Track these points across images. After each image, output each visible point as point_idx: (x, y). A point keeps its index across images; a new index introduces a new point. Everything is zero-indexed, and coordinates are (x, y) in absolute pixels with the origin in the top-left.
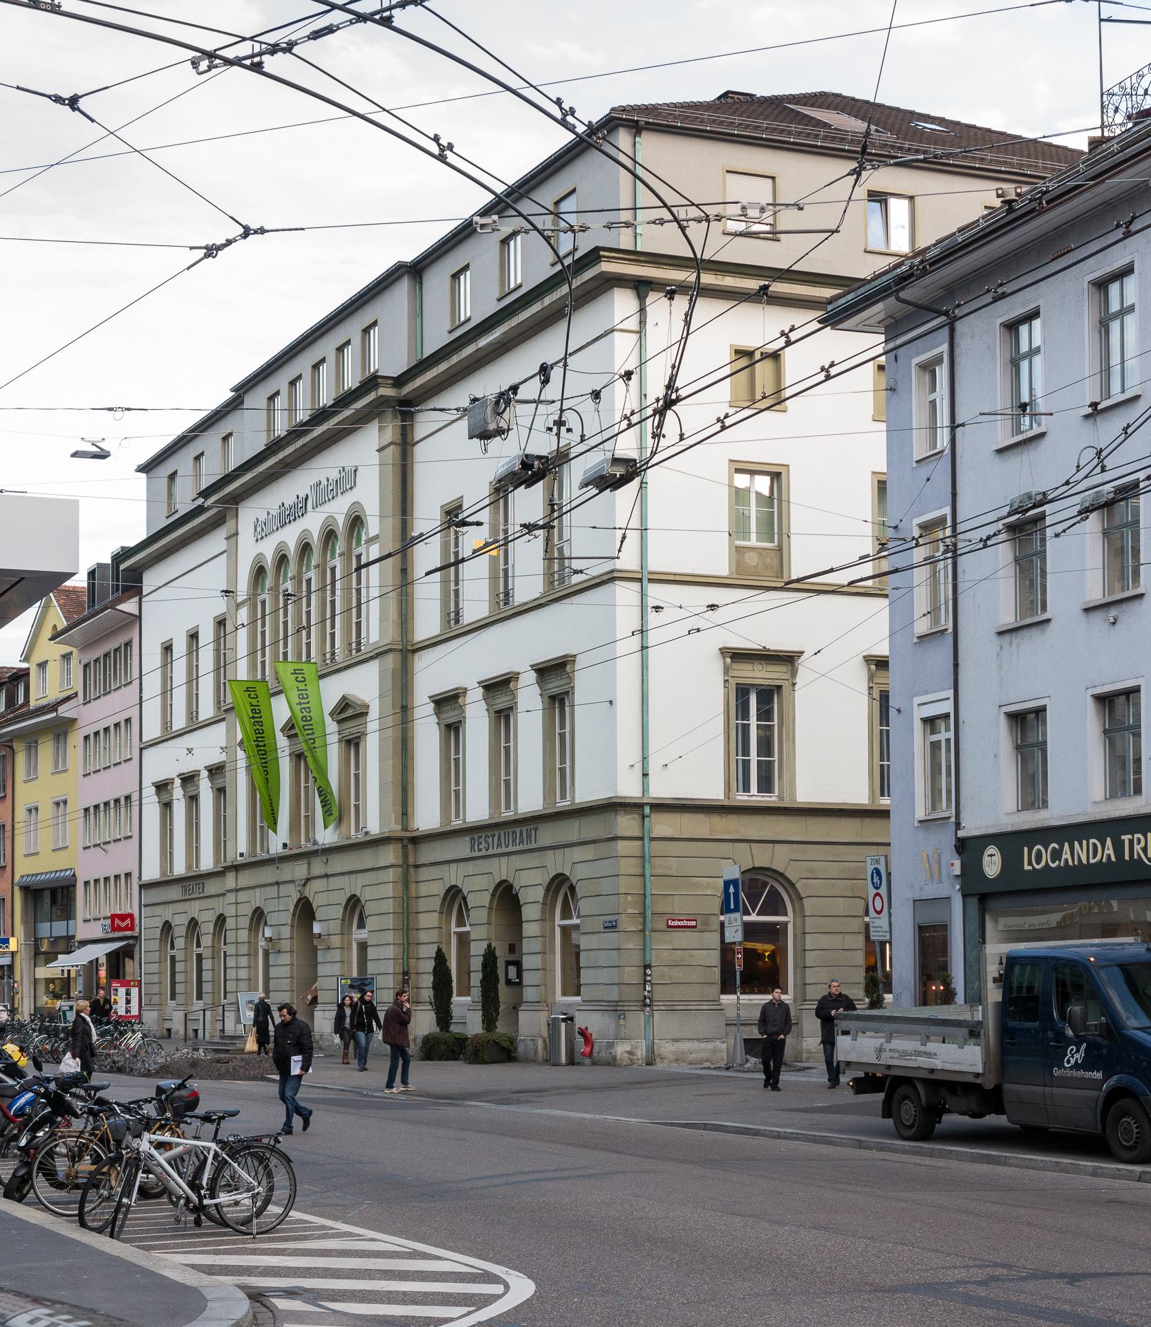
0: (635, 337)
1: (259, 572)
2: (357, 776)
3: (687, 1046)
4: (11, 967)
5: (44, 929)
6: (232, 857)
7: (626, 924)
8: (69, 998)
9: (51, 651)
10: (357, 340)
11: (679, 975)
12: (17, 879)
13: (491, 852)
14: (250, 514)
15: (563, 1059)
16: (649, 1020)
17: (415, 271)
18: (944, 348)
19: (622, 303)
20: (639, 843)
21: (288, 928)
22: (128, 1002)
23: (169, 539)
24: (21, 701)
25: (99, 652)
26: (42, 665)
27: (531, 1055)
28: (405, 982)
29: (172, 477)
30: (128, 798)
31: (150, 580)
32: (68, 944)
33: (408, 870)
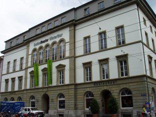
1: (35, 50)
33: (76, 89)
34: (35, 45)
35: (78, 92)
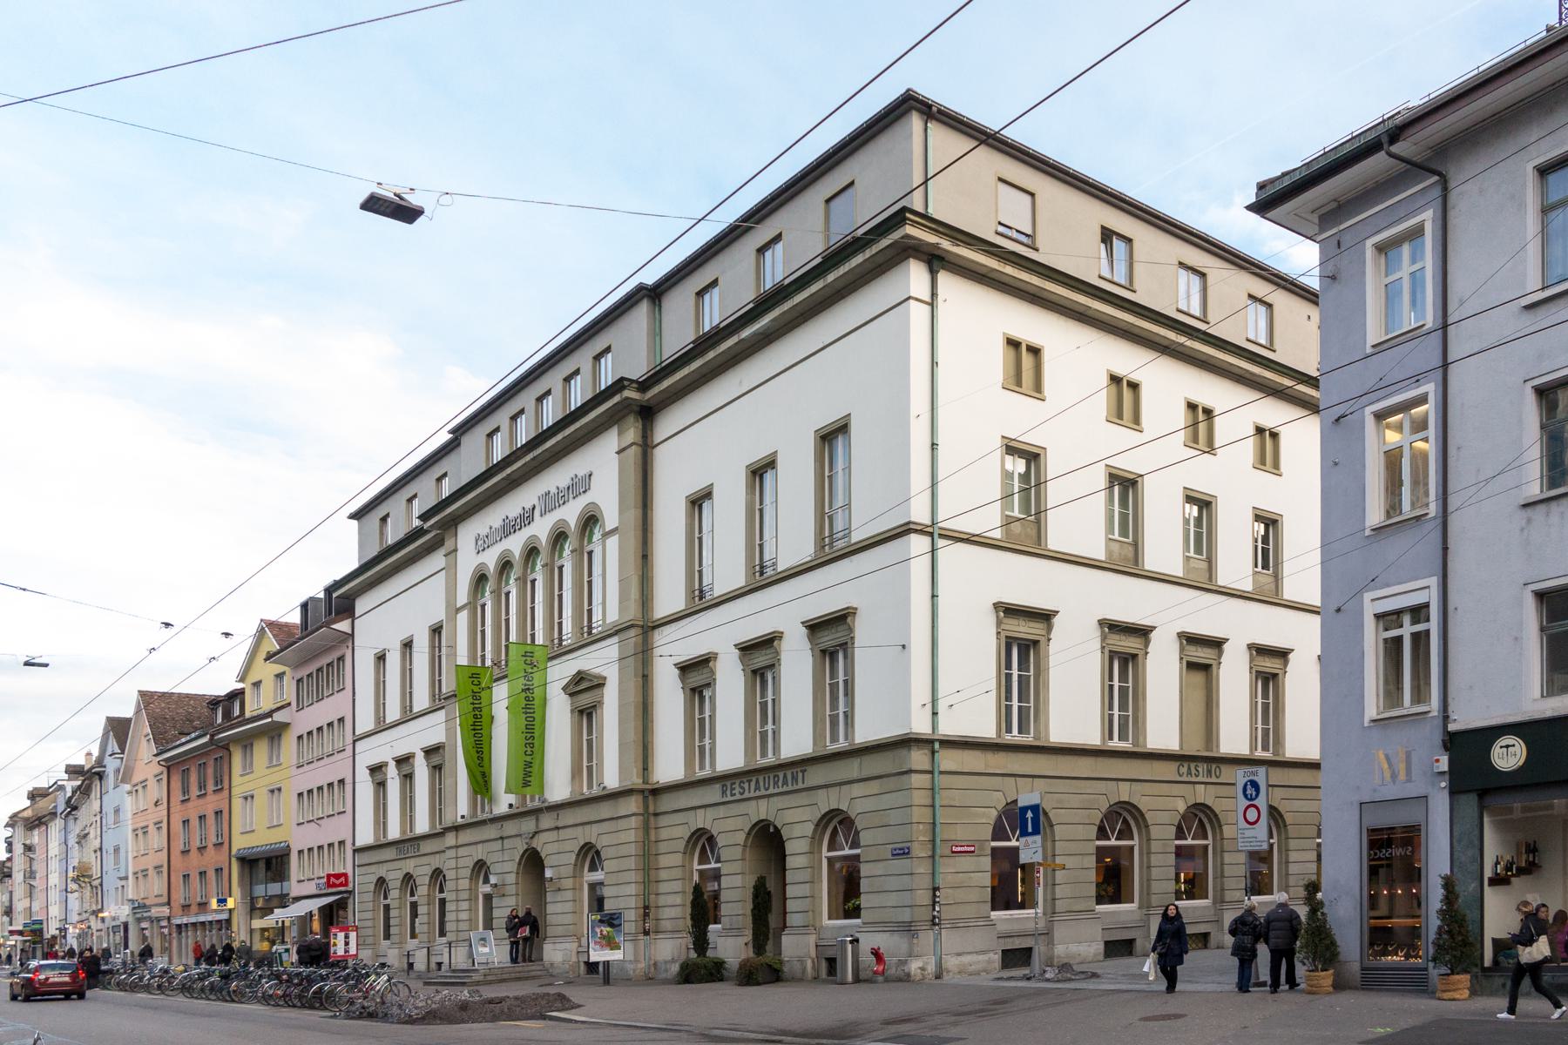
0: (928, 308)
1: (480, 579)
2: (590, 742)
3: (966, 959)
4: (228, 921)
5: (260, 890)
6: (448, 820)
7: (920, 851)
8: (283, 942)
9: (265, 671)
10: (558, 387)
11: (960, 895)
12: (234, 851)
13: (746, 795)
14: (468, 534)
15: (850, 978)
16: (938, 938)
17: (654, 294)
18: (1428, 217)
19: (916, 276)
20: (929, 776)
21: (513, 876)
22: (347, 944)
23: (379, 568)
24: (237, 712)
25: (312, 668)
26: (257, 684)
27: (799, 975)
28: (646, 915)
29: (384, 519)
30: (341, 782)
31: (361, 605)
32: (283, 901)
33: (649, 818)
34: (483, 544)
35: (664, 834)
